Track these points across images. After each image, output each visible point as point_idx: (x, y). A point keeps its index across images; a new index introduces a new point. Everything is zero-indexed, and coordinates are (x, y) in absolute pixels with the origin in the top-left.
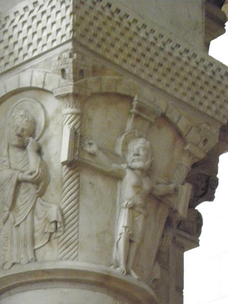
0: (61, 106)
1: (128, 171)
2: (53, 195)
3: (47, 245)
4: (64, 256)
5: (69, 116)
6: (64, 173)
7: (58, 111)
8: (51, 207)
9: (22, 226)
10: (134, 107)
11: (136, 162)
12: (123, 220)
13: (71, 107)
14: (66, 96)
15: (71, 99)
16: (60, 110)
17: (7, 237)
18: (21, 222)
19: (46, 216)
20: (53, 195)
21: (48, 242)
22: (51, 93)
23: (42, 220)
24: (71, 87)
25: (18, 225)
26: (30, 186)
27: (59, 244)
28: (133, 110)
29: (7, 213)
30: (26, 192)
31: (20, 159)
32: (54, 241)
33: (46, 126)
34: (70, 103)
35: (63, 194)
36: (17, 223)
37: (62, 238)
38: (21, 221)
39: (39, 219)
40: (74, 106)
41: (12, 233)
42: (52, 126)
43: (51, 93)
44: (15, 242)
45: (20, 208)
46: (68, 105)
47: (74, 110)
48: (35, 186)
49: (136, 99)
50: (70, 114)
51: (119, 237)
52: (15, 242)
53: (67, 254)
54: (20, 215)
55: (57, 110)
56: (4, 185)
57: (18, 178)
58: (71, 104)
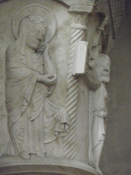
0: (71, 19)
1: (102, 84)
2: (58, 98)
3: (54, 142)
4: (67, 154)
5: (78, 31)
6: (69, 81)
7: (68, 23)
8: (59, 109)
9: (36, 121)
10: (103, 25)
11: (104, 76)
12: (100, 130)
13: (82, 23)
14: (82, 14)
15: (85, 17)
16: (69, 23)
17: (23, 129)
18: (36, 118)
19: (55, 116)
20: (58, 98)
21: (55, 139)
22: (68, 7)
23: (51, 119)
24: (92, 7)
25: (33, 120)
26: (43, 86)
27: (64, 142)
28: (102, 28)
29: (25, 107)
30: (40, 91)
31: (35, 61)
32: (60, 140)
33: (56, 34)
34: (82, 20)
35: (67, 99)
36: (33, 118)
37: (66, 138)
38: (36, 117)
39: (48, 117)
40: (84, 23)
41: (28, 126)
42: (60, 35)
43: (68, 7)
44: (31, 134)
45: (35, 105)
46: (80, 21)
47: (83, 27)
48: (47, 87)
49: (107, 18)
50: (80, 29)
51: (99, 143)
52: (31, 134)
53: (70, 152)
54: (35, 111)
55: (67, 22)
56: (23, 82)
57: (37, 79)
58: (83, 21)
